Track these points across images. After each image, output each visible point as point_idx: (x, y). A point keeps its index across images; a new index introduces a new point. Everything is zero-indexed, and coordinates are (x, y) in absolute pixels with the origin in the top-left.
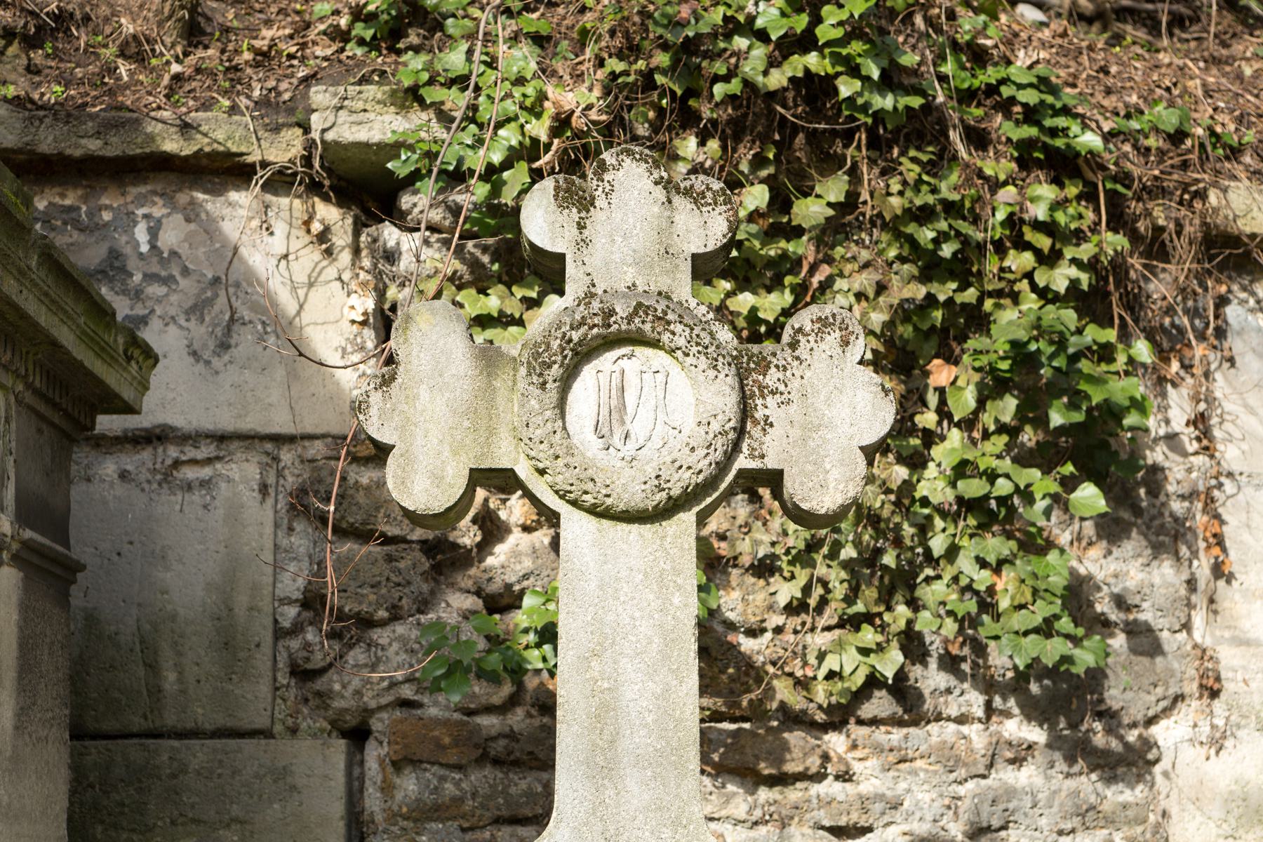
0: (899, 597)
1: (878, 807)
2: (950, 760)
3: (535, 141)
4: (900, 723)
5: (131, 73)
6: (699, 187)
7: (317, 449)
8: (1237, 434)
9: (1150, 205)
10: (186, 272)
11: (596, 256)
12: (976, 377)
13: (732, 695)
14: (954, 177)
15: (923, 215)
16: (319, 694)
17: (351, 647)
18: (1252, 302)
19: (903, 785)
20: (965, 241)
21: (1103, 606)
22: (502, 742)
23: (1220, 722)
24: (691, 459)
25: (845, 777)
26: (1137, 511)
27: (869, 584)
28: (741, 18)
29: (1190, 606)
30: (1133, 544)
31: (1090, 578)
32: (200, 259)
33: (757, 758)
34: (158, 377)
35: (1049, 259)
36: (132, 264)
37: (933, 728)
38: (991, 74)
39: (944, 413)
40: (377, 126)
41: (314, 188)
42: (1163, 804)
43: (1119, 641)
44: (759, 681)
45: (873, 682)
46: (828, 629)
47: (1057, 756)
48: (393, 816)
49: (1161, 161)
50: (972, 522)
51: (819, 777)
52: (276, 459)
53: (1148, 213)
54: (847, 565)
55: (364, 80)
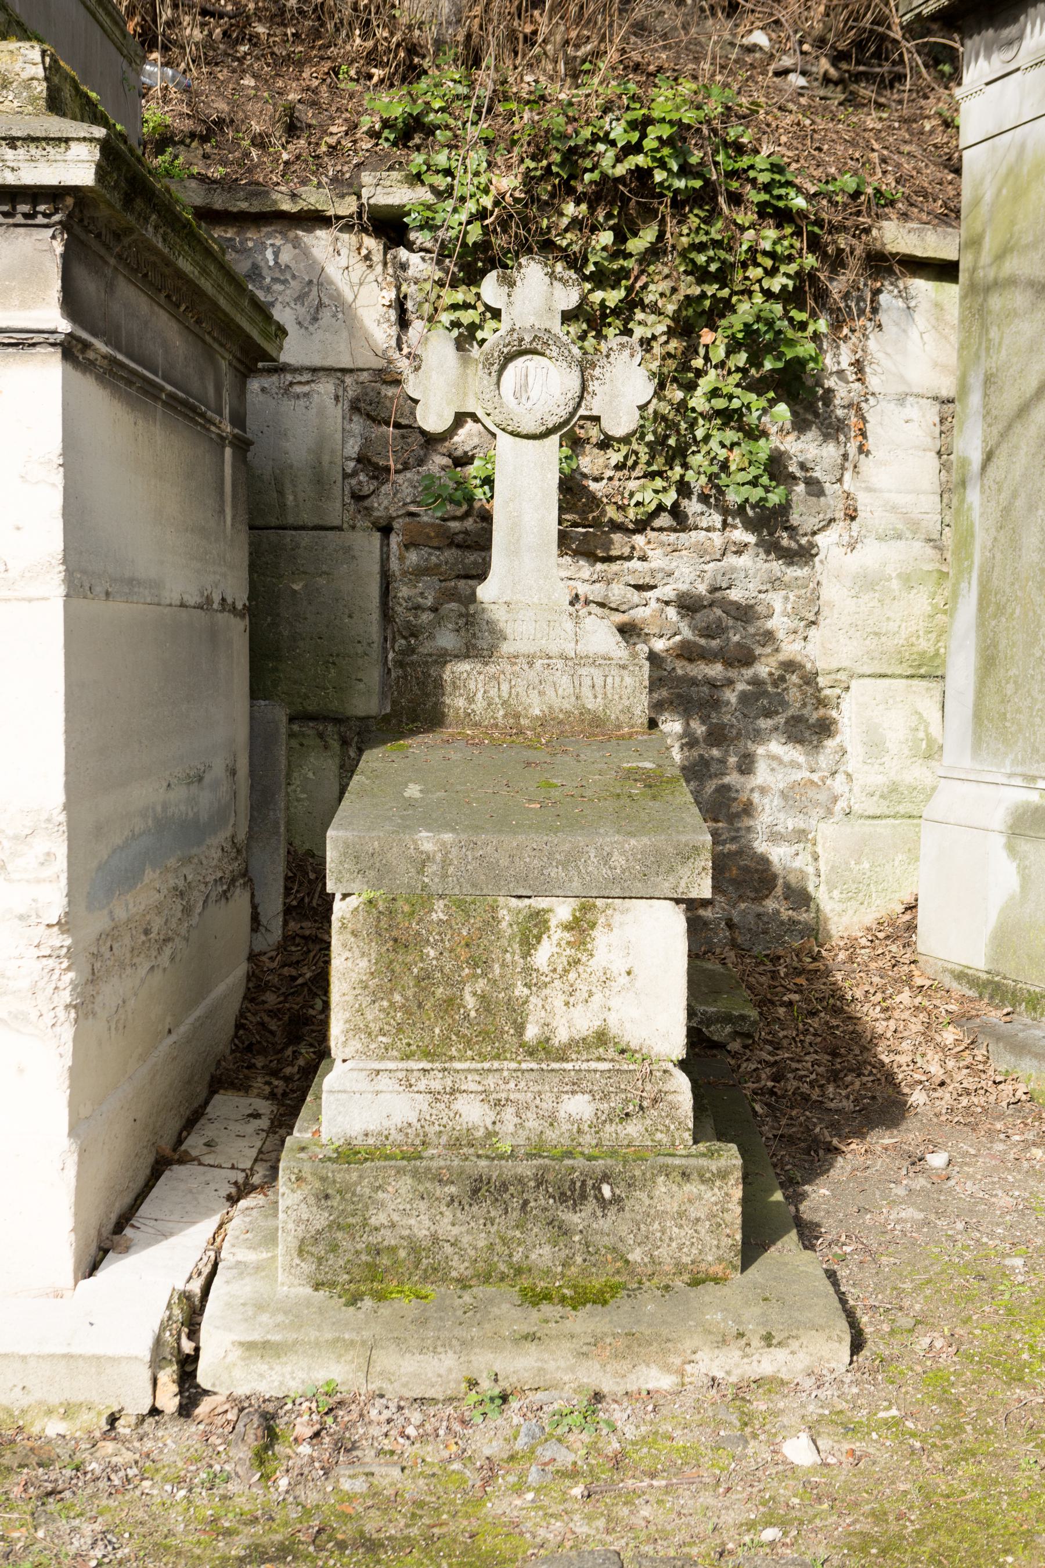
0: (677, 462)
1: (660, 575)
2: (701, 552)
3: (485, 209)
4: (675, 530)
5: (259, 156)
6: (566, 277)
7: (364, 376)
8: (879, 370)
9: (836, 237)
10: (294, 277)
11: (516, 310)
12: (726, 341)
13: (583, 513)
14: (719, 225)
15: (701, 248)
16: (366, 508)
17: (383, 484)
18: (896, 291)
19: (674, 564)
20: (724, 262)
21: (793, 468)
22: (461, 536)
23: (855, 534)
24: (558, 411)
25: (643, 558)
26: (816, 415)
27: (661, 455)
28: (601, 134)
29: (843, 468)
30: (813, 434)
31: (786, 452)
32: (299, 268)
33: (596, 547)
34: (288, 343)
35: (771, 273)
36: (265, 272)
37: (693, 533)
38: (745, 162)
39: (707, 359)
40: (398, 195)
41: (364, 230)
42: (819, 578)
43: (800, 488)
44: (598, 506)
45: (660, 508)
46: (638, 478)
47: (761, 550)
48: (405, 573)
49: (845, 210)
50: (719, 421)
51: (629, 558)
52: (343, 382)
53: (834, 242)
54: (649, 444)
55: (391, 168)
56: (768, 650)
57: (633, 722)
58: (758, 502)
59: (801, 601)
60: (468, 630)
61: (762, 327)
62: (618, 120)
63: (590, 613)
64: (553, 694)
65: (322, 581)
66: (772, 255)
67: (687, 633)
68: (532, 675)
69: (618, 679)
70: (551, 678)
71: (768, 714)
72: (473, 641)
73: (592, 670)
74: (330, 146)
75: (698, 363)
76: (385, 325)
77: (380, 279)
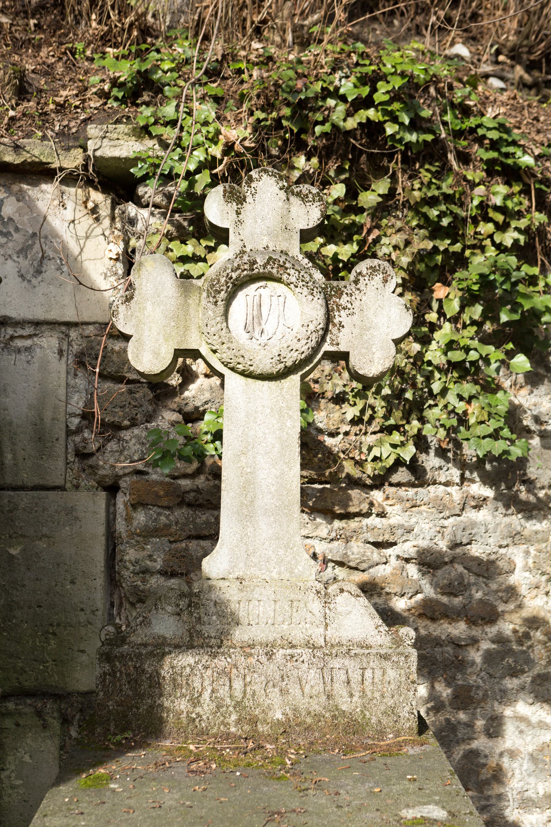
0: (414, 416)
1: (400, 532)
3: (214, 158)
4: (413, 486)
7: (90, 330)
10: (17, 230)
11: (246, 230)
12: (460, 294)
13: (320, 469)
14: (450, 181)
15: (432, 202)
16: (91, 467)
19: (414, 520)
20: (455, 216)
21: (528, 422)
24: (298, 346)
25: (382, 515)
27: (397, 409)
28: (331, 89)
31: (520, 406)
32: (24, 221)
33: (334, 504)
35: (502, 228)
37: (432, 488)
38: (472, 122)
39: (441, 313)
40: (125, 148)
41: (89, 183)
43: (536, 441)
44: (335, 462)
45: (399, 463)
46: (374, 433)
47: (500, 504)
48: (132, 535)
50: (456, 375)
51: (368, 515)
52: (68, 336)
54: (385, 398)
55: (118, 122)
56: (511, 606)
57: (399, 726)
58: (500, 455)
59: (542, 555)
60: (191, 614)
61: (497, 277)
62: (347, 77)
63: (342, 591)
64: (298, 692)
65: (42, 545)
66: (502, 210)
67: (429, 591)
68: (271, 669)
69: (378, 673)
70: (295, 673)
71: (514, 673)
72: (198, 627)
73: (347, 662)
74: (57, 104)
75: (432, 317)
76: (113, 279)
77: (107, 233)
